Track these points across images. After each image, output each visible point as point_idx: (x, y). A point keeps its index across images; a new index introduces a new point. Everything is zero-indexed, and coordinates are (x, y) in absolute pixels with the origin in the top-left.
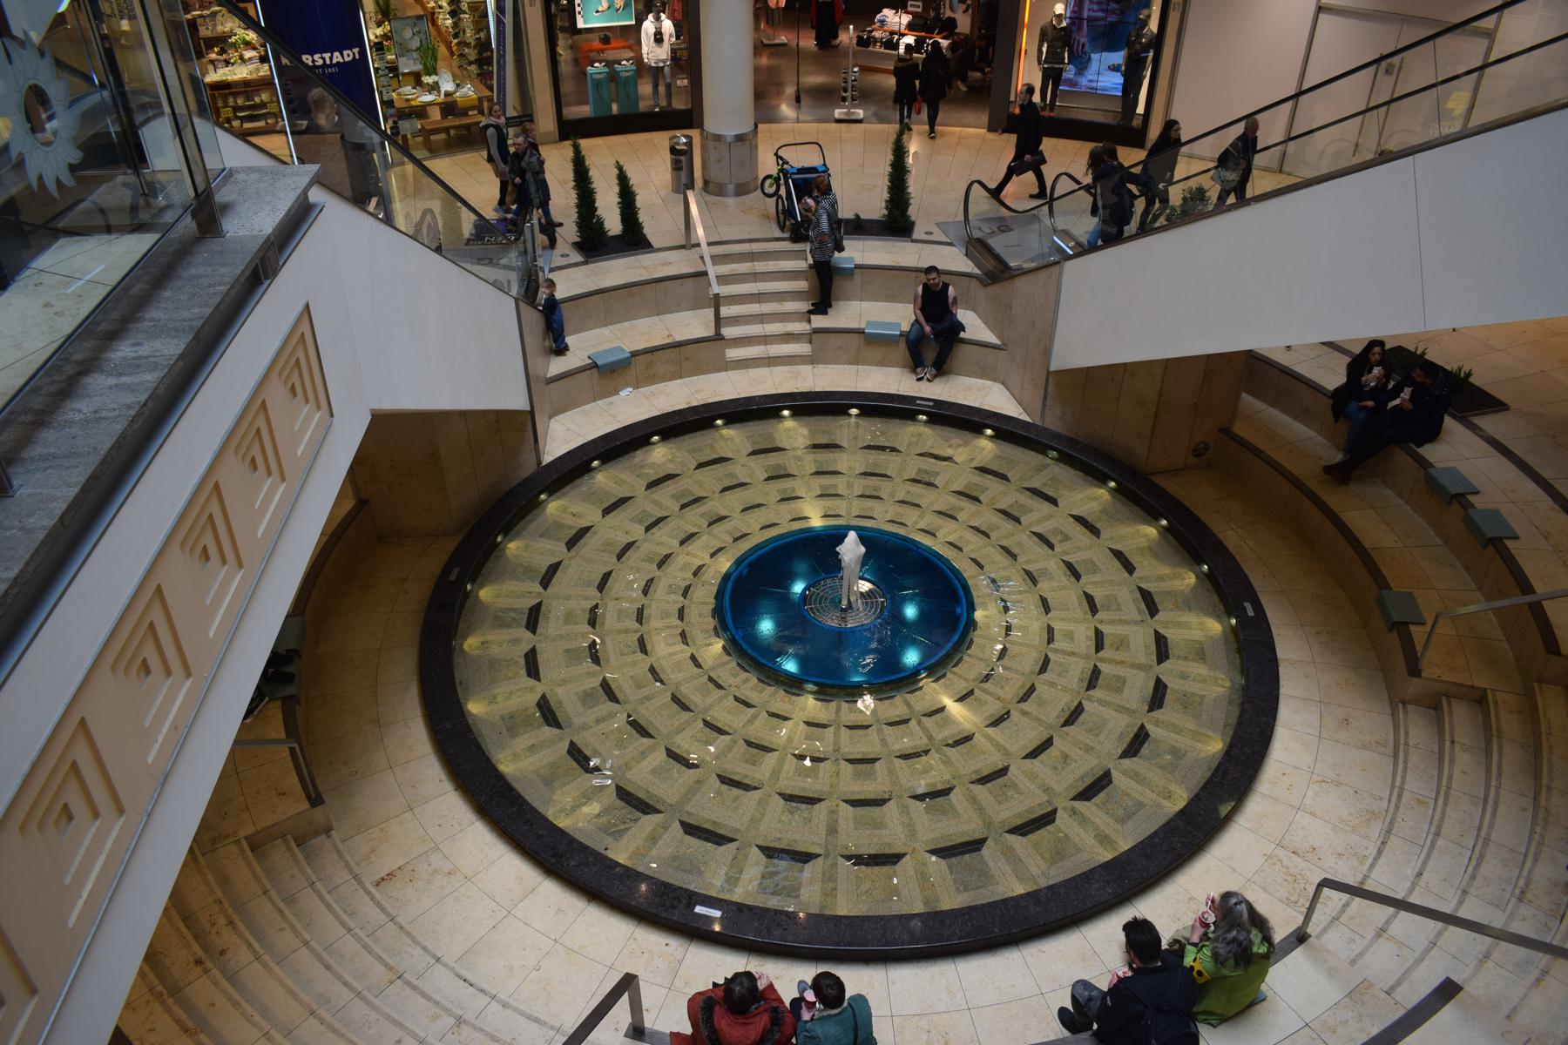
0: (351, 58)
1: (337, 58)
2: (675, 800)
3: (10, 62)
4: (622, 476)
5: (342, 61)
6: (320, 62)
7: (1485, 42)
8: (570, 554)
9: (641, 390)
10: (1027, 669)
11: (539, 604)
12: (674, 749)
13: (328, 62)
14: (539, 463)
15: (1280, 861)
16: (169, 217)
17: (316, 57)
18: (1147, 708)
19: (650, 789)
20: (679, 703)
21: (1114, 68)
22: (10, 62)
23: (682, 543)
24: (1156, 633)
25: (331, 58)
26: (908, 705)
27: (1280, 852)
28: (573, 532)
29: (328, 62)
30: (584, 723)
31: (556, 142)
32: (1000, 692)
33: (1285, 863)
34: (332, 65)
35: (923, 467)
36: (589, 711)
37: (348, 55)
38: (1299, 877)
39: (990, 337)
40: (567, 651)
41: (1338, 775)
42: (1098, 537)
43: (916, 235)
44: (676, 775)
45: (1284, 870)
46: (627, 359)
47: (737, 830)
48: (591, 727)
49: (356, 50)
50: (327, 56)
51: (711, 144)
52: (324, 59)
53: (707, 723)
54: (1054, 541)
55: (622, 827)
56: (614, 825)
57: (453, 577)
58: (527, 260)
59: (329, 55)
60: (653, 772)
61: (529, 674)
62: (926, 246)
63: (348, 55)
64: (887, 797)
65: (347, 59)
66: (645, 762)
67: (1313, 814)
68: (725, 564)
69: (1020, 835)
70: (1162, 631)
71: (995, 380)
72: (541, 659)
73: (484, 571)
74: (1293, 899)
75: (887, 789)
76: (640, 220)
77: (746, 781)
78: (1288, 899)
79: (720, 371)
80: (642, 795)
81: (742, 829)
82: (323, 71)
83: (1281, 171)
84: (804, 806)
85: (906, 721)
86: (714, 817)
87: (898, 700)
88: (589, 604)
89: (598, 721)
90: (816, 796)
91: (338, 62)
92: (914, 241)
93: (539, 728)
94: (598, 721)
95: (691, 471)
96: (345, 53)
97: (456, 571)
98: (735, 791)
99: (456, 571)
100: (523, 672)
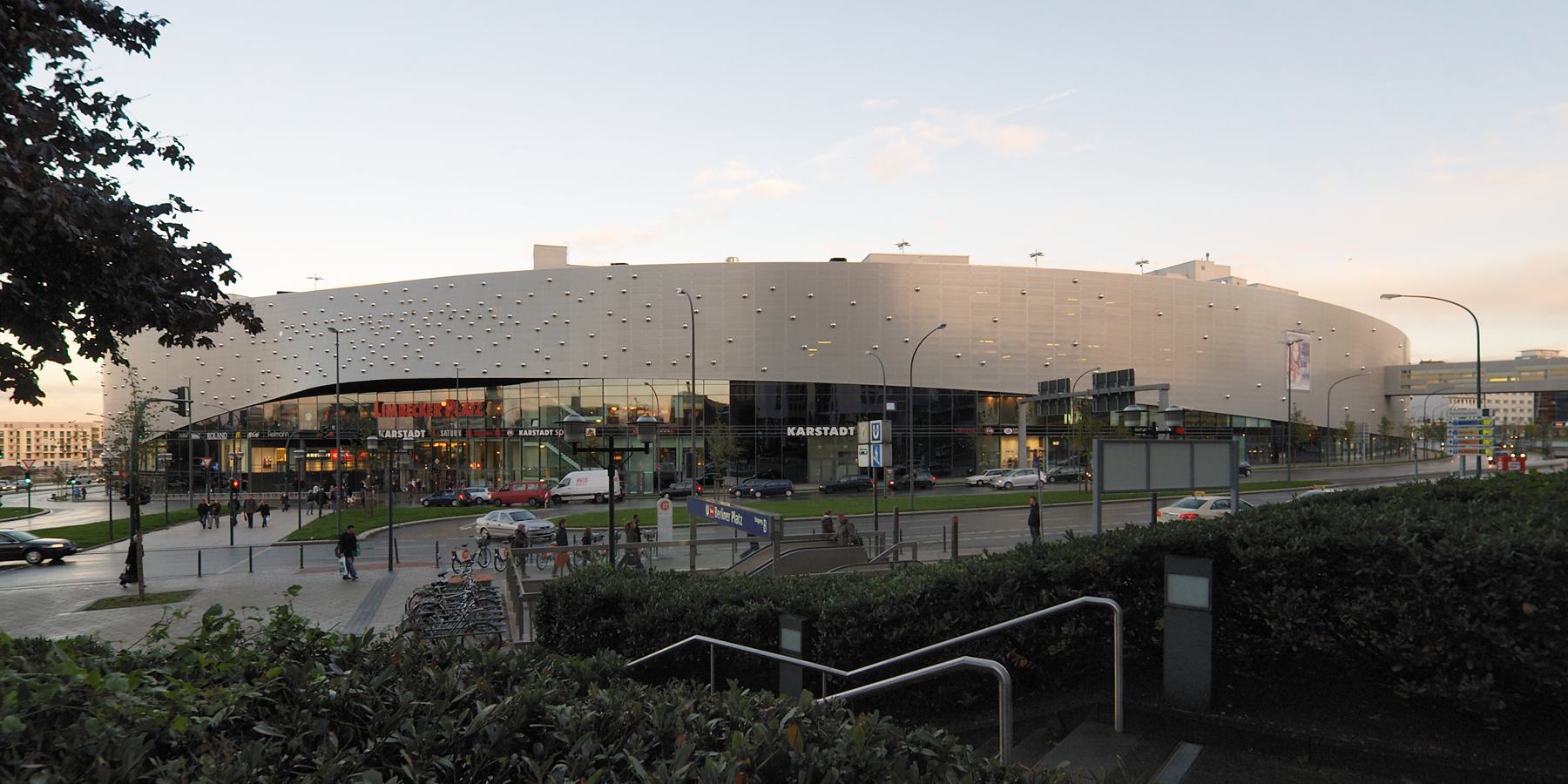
0: (846, 433)
3: (1383, 296)
13: (826, 434)
16: (1524, 532)
17: (818, 429)
21: (610, 650)
22: (1383, 296)
25: (829, 431)
29: (826, 434)
50: (826, 429)
52: (823, 431)
58: (66, 328)
59: (828, 428)
62: (253, 565)
83: (251, 547)
91: (834, 435)
96: (808, 429)
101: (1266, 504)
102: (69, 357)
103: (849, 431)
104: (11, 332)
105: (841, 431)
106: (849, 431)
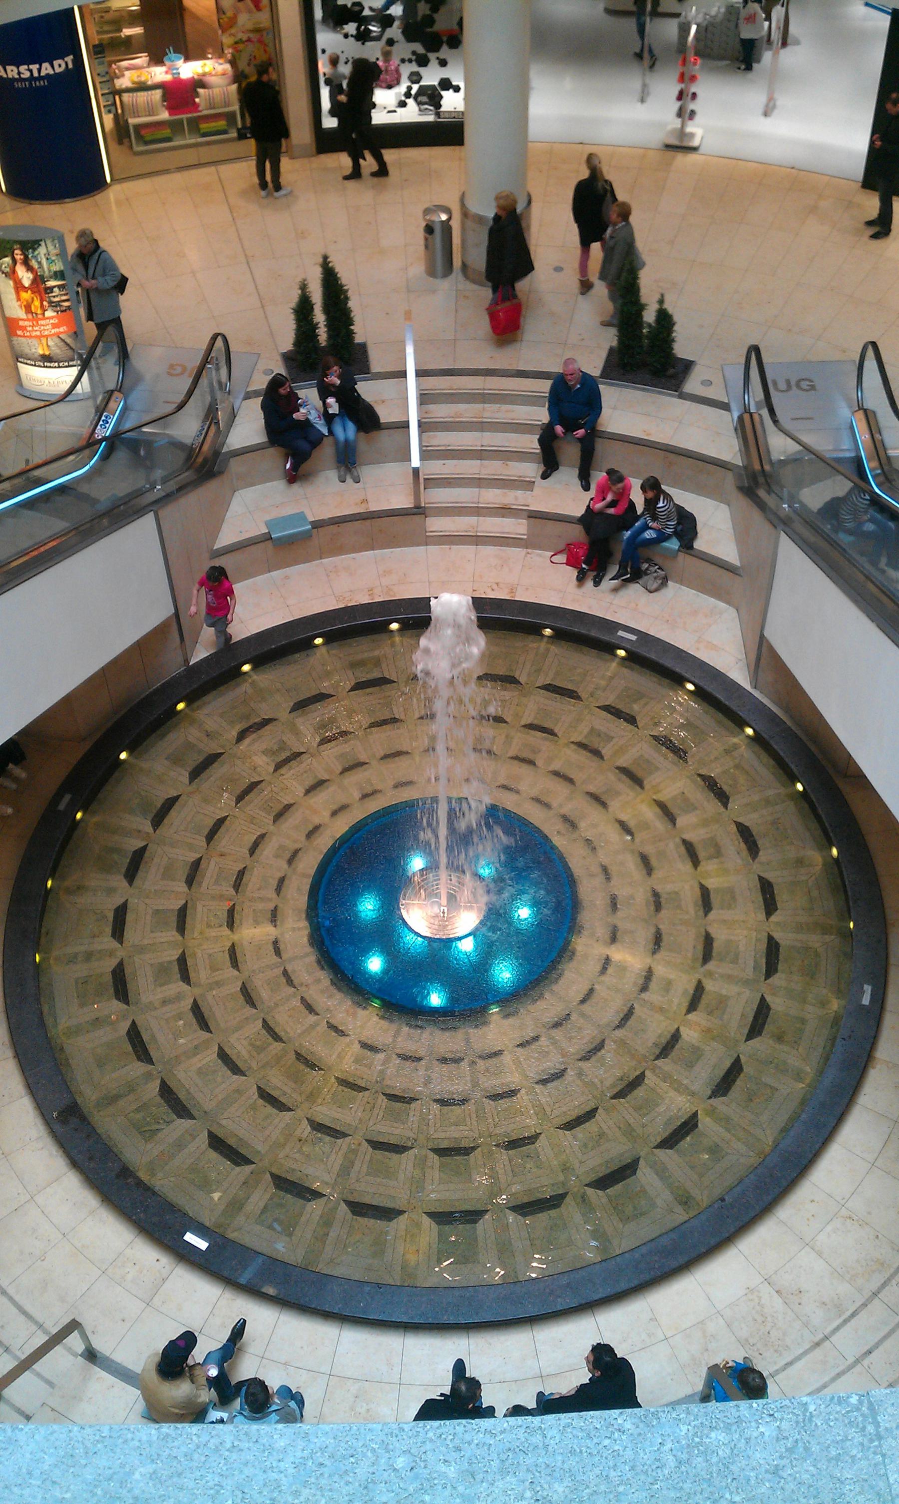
1: (46, 69)
2: (210, 1107)
3: (793, 419)
4: (70, 950)
5: (52, 72)
6: (27, 75)
7: (76, 1334)
8: (190, 789)
9: (325, 561)
10: (604, 1021)
11: (144, 849)
12: (226, 1049)
13: (36, 74)
14: (187, 661)
15: (760, 1298)
17: (23, 68)
18: (709, 1092)
19: (192, 1091)
20: (248, 996)
22: (793, 419)
23: (308, 792)
24: (763, 999)
25: (39, 70)
26: (467, 1041)
27: (766, 1290)
28: (201, 759)
29: (36, 74)
30: (150, 1003)
31: (313, 156)
32: (564, 1044)
33: (763, 1301)
34: (40, 78)
35: (597, 727)
36: (159, 990)
37: (59, 66)
38: (769, 1319)
39: (728, 552)
40: (157, 912)
41: (869, 1213)
42: (754, 859)
43: (692, 385)
44: (219, 1079)
45: (758, 1308)
46: (308, 531)
47: (258, 1152)
48: (156, 1008)
49: (69, 59)
50: (35, 67)
51: (469, 223)
52: (31, 71)
53: (266, 1025)
54: (702, 854)
55: (157, 1127)
56: (149, 1124)
57: (62, 807)
59: (37, 66)
60: (200, 1072)
61: (113, 935)
63: (59, 66)
64: (410, 1144)
65: (58, 70)
66: (195, 1060)
67: (820, 1254)
68: (341, 826)
69: (520, 1214)
70: (768, 998)
71: (728, 603)
72: (130, 917)
73: (100, 796)
74: (751, 1341)
75: (412, 1135)
76: (358, 339)
77: (283, 1099)
78: (747, 1340)
79: (418, 545)
80: (182, 1096)
81: (262, 1152)
82: (31, 84)
84: (327, 1139)
85: (457, 1061)
86: (241, 1133)
87: (460, 1035)
88: (193, 856)
89: (164, 1002)
90: (342, 1129)
91: (48, 75)
92: (683, 396)
93: (108, 1000)
94: (164, 1002)
95: (345, 693)
96: (56, 63)
97: (67, 798)
98: (270, 1109)
99: (67, 798)
100: (109, 930)
101: (400, 31)
102: (586, 510)
103: (66, 64)
104: (353, 325)
105: (56, 67)
106: (66, 64)
